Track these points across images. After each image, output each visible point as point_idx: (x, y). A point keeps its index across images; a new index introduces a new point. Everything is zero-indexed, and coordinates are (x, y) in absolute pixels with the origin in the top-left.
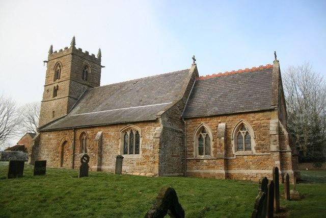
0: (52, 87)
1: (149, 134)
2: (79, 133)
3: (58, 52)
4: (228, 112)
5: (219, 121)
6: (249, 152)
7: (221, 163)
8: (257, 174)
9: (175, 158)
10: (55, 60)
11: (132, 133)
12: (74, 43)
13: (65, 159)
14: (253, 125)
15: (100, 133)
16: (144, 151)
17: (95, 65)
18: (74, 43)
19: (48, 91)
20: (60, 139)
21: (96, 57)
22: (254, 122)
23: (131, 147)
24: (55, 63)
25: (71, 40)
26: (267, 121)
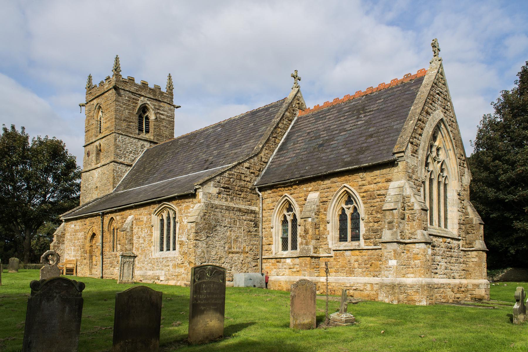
0: (92, 148)
2: (107, 219)
3: (98, 86)
4: (323, 170)
5: (310, 189)
6: (354, 244)
7: (306, 265)
8: (365, 284)
9: (236, 256)
10: (95, 101)
12: (117, 69)
13: (94, 263)
14: (362, 194)
15: (130, 218)
16: (182, 244)
17: (162, 104)
18: (117, 69)
19: (88, 154)
20: (87, 231)
21: (164, 90)
22: (365, 188)
24: (95, 105)
25: (112, 64)
26: (385, 184)
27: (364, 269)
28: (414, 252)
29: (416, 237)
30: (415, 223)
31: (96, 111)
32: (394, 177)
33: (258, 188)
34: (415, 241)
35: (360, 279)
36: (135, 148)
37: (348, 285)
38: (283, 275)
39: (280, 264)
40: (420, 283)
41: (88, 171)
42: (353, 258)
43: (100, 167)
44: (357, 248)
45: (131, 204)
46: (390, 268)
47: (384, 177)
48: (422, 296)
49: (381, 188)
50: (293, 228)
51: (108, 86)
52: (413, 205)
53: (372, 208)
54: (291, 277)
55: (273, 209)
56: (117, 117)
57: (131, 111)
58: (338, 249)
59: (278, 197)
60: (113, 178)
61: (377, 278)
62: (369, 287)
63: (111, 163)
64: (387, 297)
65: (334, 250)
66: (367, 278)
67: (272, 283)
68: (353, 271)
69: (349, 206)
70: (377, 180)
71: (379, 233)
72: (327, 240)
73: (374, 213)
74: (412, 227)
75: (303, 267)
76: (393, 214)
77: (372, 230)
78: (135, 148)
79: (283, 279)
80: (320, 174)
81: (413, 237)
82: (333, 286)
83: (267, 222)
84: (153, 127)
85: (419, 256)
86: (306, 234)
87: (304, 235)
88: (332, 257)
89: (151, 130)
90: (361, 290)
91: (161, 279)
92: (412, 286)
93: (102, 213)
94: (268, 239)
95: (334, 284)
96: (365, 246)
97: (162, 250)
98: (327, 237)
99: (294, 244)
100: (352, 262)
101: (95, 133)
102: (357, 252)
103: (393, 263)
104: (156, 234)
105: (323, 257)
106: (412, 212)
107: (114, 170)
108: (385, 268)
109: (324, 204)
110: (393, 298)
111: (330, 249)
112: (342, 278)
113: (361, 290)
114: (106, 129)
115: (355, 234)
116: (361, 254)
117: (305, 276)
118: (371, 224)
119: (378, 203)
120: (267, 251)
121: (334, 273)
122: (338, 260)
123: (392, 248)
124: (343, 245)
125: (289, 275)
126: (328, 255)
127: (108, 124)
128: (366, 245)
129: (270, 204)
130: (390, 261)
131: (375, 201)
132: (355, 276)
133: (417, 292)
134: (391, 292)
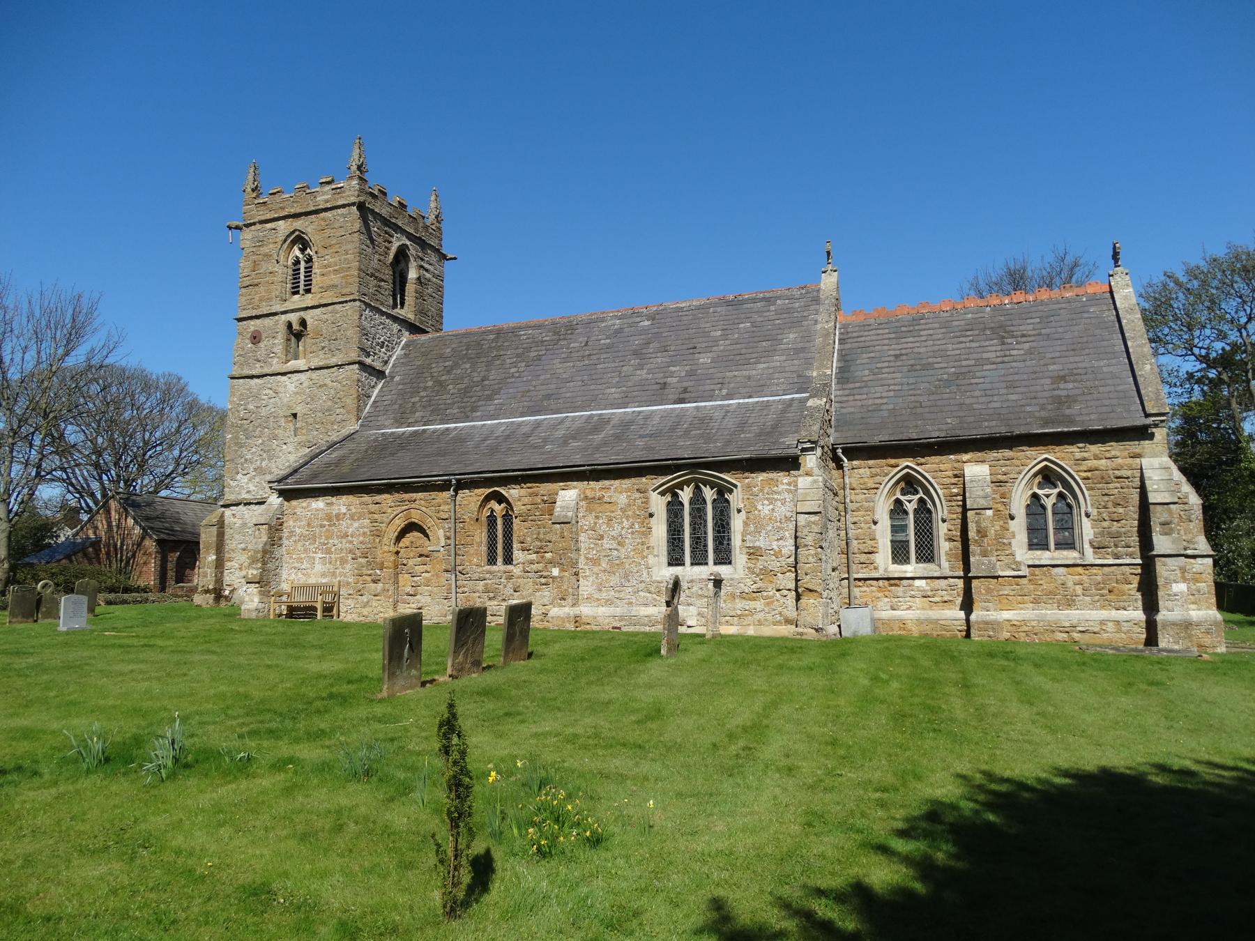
1: (771, 501)
6: (1070, 556)
8: (1102, 622)
11: (698, 499)
16: (754, 553)
22: (1090, 464)
23: (699, 543)
27: (1097, 598)
28: (1194, 570)
29: (1196, 546)
30: (1192, 525)
31: (285, 246)
32: (1145, 450)
33: (841, 448)
34: (1196, 552)
35: (1090, 614)
36: (388, 335)
37: (1067, 624)
38: (909, 608)
39: (900, 589)
40: (1213, 619)
41: (258, 377)
42: (1070, 581)
43: (307, 371)
44: (1079, 562)
45: (584, 466)
46: (1175, 595)
47: (1126, 449)
48: (1219, 639)
49: (1122, 467)
50: (918, 525)
51: (330, 196)
52: (1186, 497)
53: (1106, 498)
54: (930, 613)
55: (877, 488)
56: (362, 267)
57: (382, 258)
58: (1038, 563)
59: (885, 468)
60: (357, 398)
61: (1125, 612)
62: (1110, 627)
63: (348, 364)
64: (1178, 643)
65: (1029, 566)
66: (1103, 612)
67: (883, 624)
68: (1074, 601)
69: (1047, 491)
70: (1113, 453)
71: (1124, 539)
72: (1011, 548)
73: (1110, 505)
74: (1187, 531)
75: (982, 594)
76: (1170, 512)
77: (1109, 533)
78: (388, 335)
79: (911, 616)
80: (998, 435)
81: (1192, 546)
82: (1033, 627)
83: (860, 511)
84: (414, 294)
85: (1203, 576)
86: (982, 537)
87: (977, 538)
88: (1025, 577)
89: (410, 298)
90: (1094, 633)
91: (689, 623)
92: (1198, 624)
93: (457, 480)
94: (864, 543)
95: (1034, 624)
96: (1095, 558)
97: (492, 560)
98: (1010, 544)
99: (922, 552)
100: (1070, 584)
101: (282, 293)
102: (1080, 569)
103: (1180, 587)
104: (660, 530)
105: (1003, 577)
106: (1186, 507)
107: (359, 381)
108: (1166, 596)
109: (1001, 486)
110: (1189, 644)
111: (1020, 563)
112: (1049, 612)
113: (1094, 633)
114: (325, 289)
115: (1061, 538)
116: (1087, 572)
117: (988, 611)
118: (1106, 524)
119: (1117, 490)
120: (864, 565)
121: (1031, 605)
122: (1040, 582)
123: (1176, 564)
124: (1045, 557)
125: (923, 609)
126: (1016, 573)
127: (335, 279)
128: (1096, 557)
129: (866, 480)
130: (1174, 585)
131: (1111, 486)
132: (1078, 609)
133: (1208, 632)
134: (1182, 635)
